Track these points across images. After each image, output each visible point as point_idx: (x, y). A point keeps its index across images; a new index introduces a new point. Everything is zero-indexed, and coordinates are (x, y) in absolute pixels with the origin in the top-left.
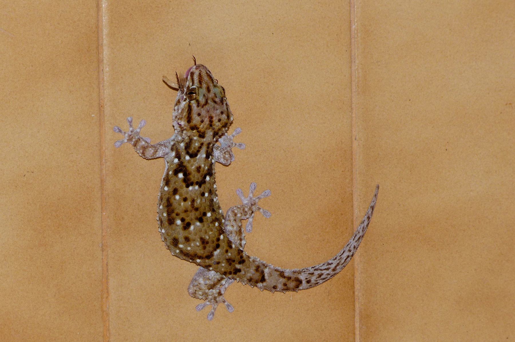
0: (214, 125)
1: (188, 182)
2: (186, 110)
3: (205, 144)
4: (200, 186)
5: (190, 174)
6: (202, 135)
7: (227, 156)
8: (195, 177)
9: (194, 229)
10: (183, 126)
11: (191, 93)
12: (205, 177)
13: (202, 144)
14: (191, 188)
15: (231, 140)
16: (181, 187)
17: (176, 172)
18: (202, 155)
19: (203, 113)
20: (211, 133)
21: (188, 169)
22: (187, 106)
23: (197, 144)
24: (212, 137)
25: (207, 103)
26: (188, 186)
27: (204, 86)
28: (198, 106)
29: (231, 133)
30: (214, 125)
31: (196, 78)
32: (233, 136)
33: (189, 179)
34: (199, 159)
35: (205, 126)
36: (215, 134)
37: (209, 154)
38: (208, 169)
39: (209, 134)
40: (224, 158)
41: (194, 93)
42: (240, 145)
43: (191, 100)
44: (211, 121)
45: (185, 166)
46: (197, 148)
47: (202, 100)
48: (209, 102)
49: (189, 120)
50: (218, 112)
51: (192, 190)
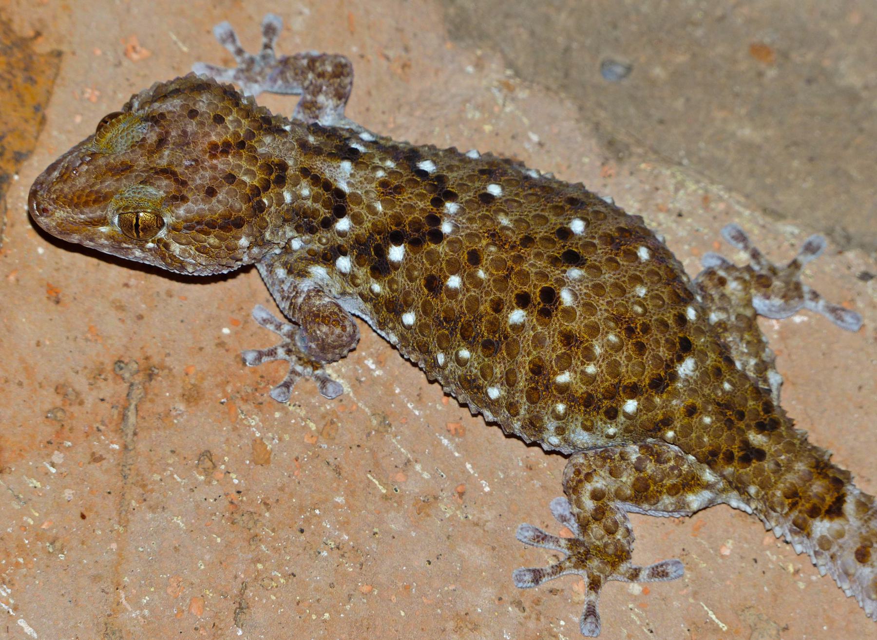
0: (236, 134)
1: (422, 234)
9: (575, 295)
12: (424, 174)
13: (305, 172)
14: (446, 228)
17: (381, 268)
18: (342, 175)
19: (201, 178)
23: (306, 192)
25: (167, 172)
26: (438, 237)
27: (109, 185)
28: (184, 199)
30: (236, 134)
33: (416, 225)
38: (395, 159)
44: (226, 148)
47: (157, 191)
48: (164, 163)
50: (192, 127)
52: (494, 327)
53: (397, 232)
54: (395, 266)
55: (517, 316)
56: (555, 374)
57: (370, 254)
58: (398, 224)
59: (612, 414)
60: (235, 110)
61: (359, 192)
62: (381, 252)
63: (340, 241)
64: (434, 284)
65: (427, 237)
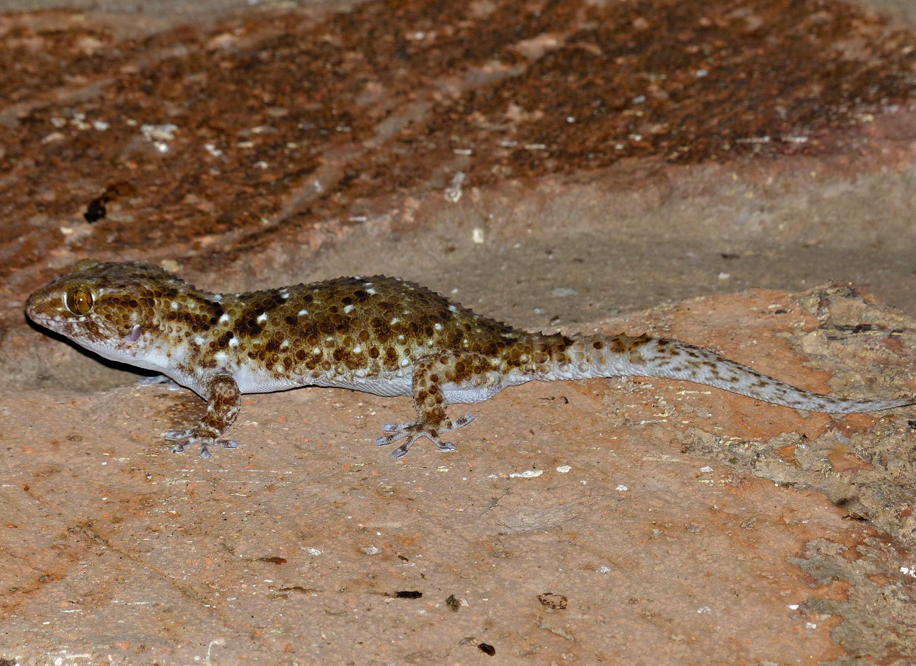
26: (284, 301)
52: (338, 318)
55: (348, 309)
56: (389, 322)
58: (257, 306)
59: (430, 332)
62: (253, 322)
63: (226, 329)
64: (292, 320)
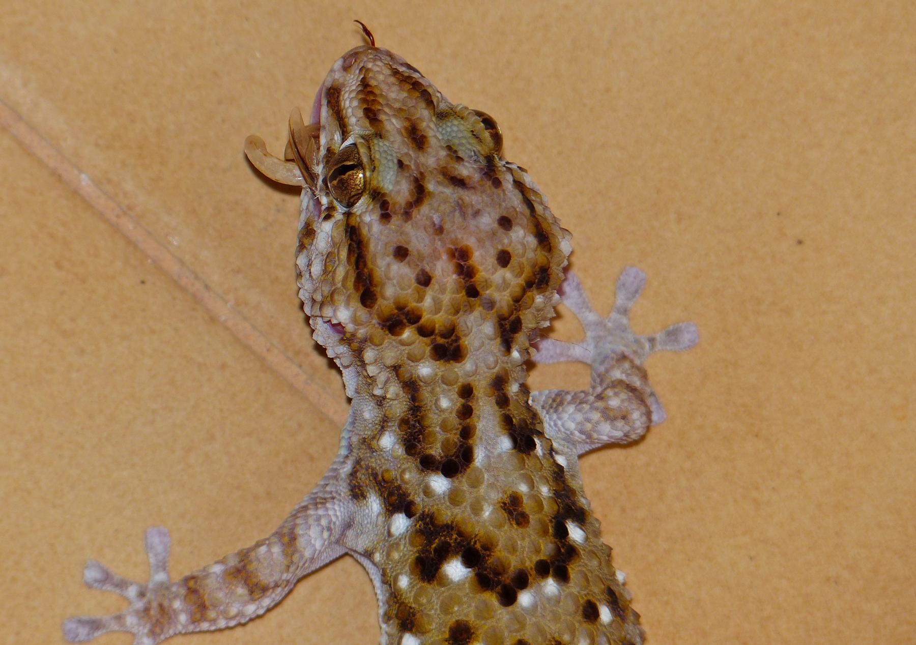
1: (503, 585)
2: (344, 254)
3: (481, 387)
4: (562, 576)
5: (488, 547)
6: (448, 349)
7: (614, 403)
8: (520, 547)
10: (350, 327)
11: (342, 166)
12: (562, 532)
13: (467, 392)
14: (525, 599)
15: (624, 329)
16: (484, 612)
17: (428, 569)
18: (492, 445)
19: (418, 239)
20: (489, 328)
21: (468, 529)
22: (340, 235)
24: (496, 346)
25: (420, 193)
26: (508, 598)
27: (393, 124)
28: (386, 217)
29: (577, 304)
31: (351, 105)
32: (625, 311)
33: (499, 571)
34: (489, 467)
35: (446, 298)
36: (508, 329)
37: (524, 436)
39: (479, 332)
40: (609, 415)
41: (352, 167)
42: (673, 334)
43: (350, 205)
44: (466, 272)
45: (449, 528)
46: (454, 420)
48: (431, 186)
49: (367, 291)
50: (488, 221)
51: (535, 606)
53: (477, 551)
54: (443, 581)
57: (430, 543)
60: (521, 281)
61: (486, 476)
62: (443, 554)
65: (499, 588)
